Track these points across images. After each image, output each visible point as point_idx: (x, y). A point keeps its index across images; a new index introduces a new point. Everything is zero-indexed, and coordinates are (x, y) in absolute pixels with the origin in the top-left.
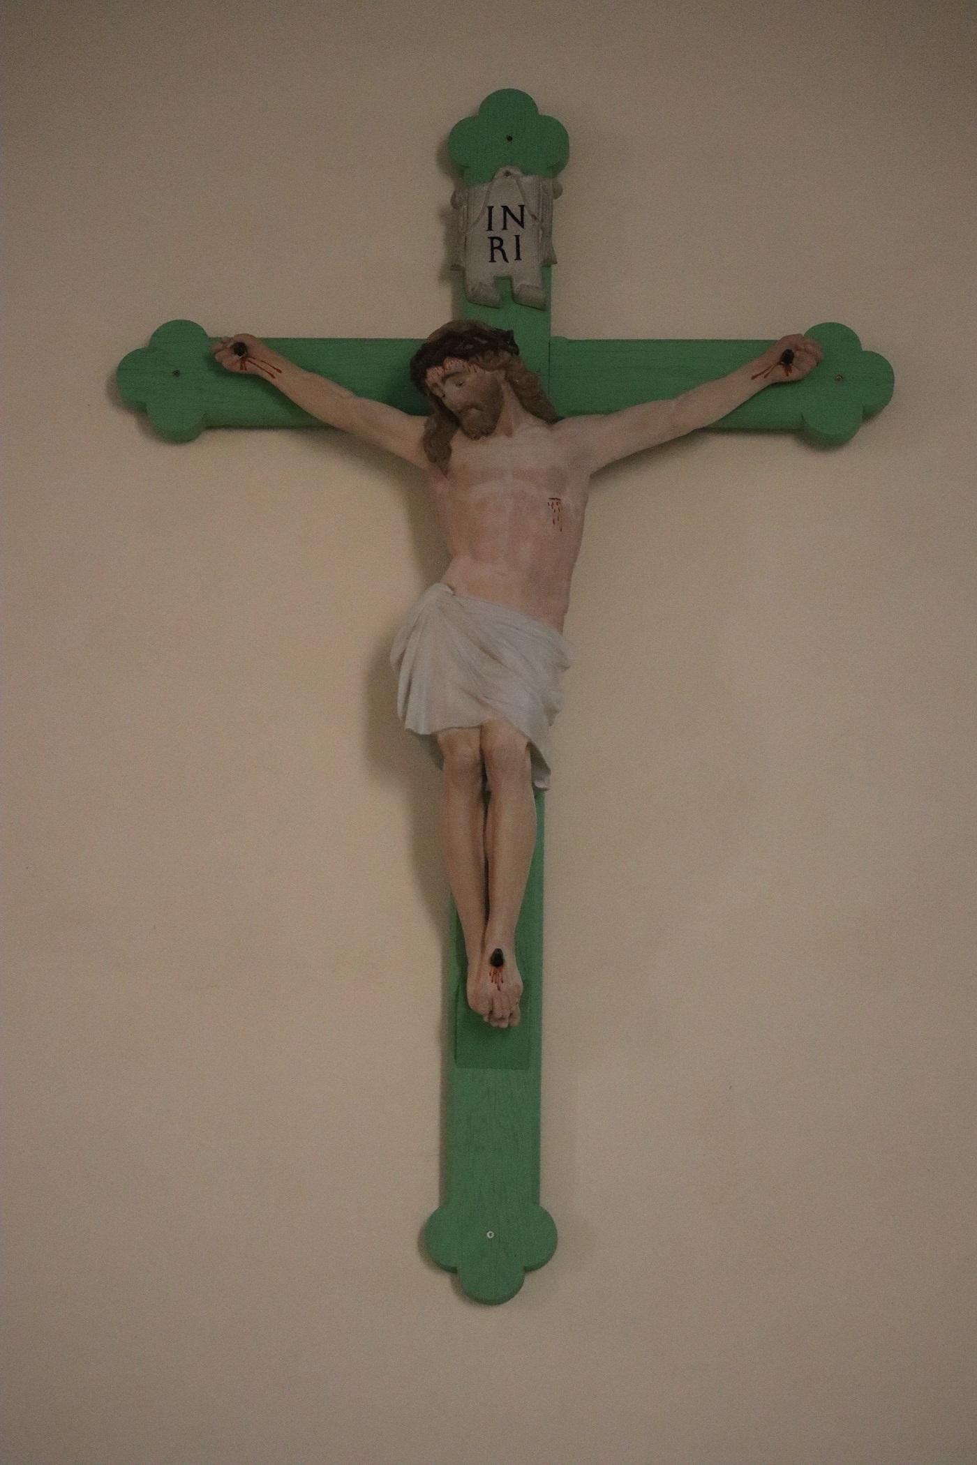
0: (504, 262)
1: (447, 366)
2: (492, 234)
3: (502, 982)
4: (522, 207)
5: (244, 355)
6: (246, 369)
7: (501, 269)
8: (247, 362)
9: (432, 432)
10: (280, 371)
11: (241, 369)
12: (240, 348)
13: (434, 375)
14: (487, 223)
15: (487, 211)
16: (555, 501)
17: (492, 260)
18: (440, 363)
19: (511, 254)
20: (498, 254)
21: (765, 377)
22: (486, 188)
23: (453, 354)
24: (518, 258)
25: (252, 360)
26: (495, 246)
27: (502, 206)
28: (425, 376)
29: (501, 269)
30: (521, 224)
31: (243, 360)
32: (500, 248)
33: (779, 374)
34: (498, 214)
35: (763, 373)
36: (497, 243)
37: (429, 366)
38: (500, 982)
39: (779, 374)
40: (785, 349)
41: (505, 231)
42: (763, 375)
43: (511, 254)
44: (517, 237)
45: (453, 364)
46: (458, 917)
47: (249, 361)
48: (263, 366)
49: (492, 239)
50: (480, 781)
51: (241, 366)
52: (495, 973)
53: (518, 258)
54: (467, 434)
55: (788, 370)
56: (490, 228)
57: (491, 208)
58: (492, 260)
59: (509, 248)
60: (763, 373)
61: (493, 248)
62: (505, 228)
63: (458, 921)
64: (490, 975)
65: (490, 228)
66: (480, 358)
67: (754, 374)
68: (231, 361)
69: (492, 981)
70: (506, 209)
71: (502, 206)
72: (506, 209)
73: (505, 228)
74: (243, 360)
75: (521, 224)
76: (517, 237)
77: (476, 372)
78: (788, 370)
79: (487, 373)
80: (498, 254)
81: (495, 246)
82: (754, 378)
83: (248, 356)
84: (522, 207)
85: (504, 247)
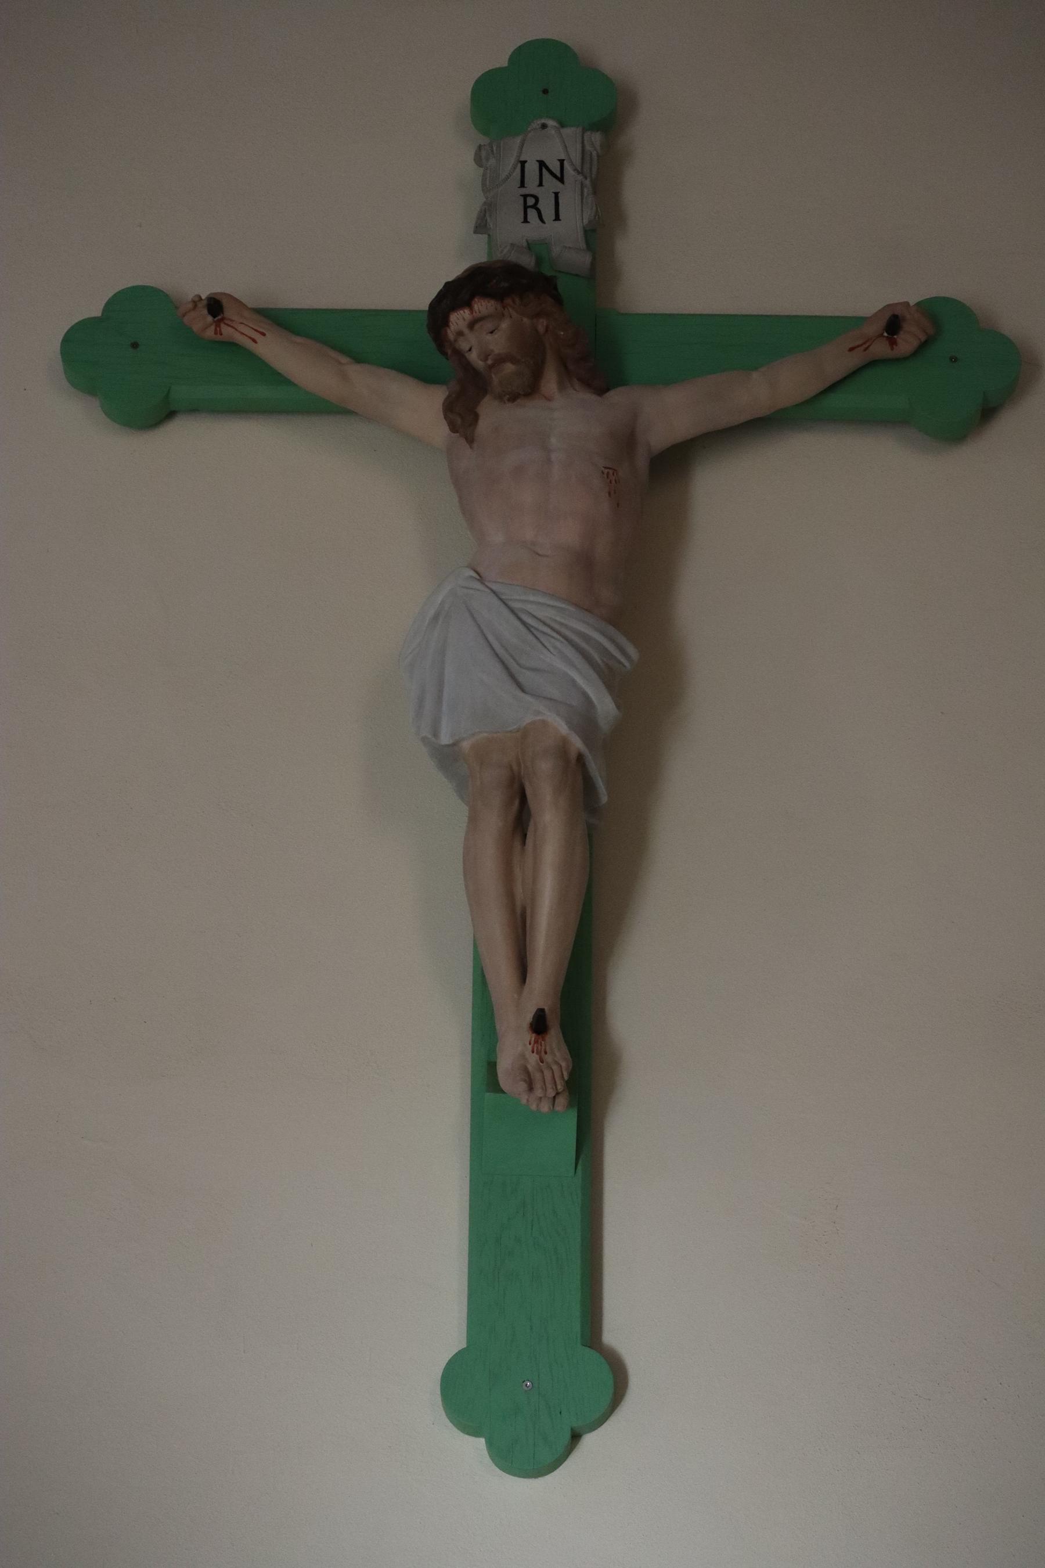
0: (540, 222)
1: (476, 307)
2: (524, 191)
3: (546, 1053)
4: (562, 162)
5: (220, 317)
6: (221, 334)
7: (534, 230)
8: (222, 325)
9: (454, 396)
10: (263, 334)
11: (216, 333)
12: (215, 306)
13: (459, 319)
14: (519, 177)
15: (519, 165)
16: (611, 472)
17: (526, 221)
18: (468, 304)
19: (548, 212)
20: (532, 214)
21: (865, 350)
22: (518, 140)
23: (487, 295)
24: (557, 218)
25: (229, 323)
26: (528, 205)
27: (537, 161)
28: (446, 323)
29: (534, 230)
30: (561, 179)
31: (218, 324)
32: (535, 206)
33: (880, 349)
34: (532, 168)
35: (861, 345)
36: (531, 201)
37: (454, 308)
38: (543, 1053)
39: (880, 349)
40: (905, 300)
41: (541, 187)
42: (862, 348)
43: (548, 212)
44: (556, 194)
45: (482, 306)
46: (482, 971)
47: (225, 324)
48: (241, 328)
49: (525, 197)
50: (517, 802)
51: (216, 330)
52: (536, 1042)
53: (557, 218)
54: (500, 398)
55: (893, 343)
56: (522, 184)
57: (523, 163)
58: (526, 221)
59: (547, 207)
60: (861, 345)
61: (526, 207)
62: (541, 184)
63: (483, 976)
64: (530, 1044)
65: (522, 184)
66: (517, 301)
67: (851, 346)
68: (203, 320)
69: (533, 1052)
70: (542, 164)
71: (537, 161)
72: (542, 164)
73: (541, 184)
74: (218, 324)
75: (561, 179)
76: (556, 194)
77: (511, 317)
78: (893, 343)
79: (425, 628)
80: (532, 214)
81: (528, 205)
82: (851, 349)
83: (222, 319)
84: (562, 162)
85: (540, 206)
